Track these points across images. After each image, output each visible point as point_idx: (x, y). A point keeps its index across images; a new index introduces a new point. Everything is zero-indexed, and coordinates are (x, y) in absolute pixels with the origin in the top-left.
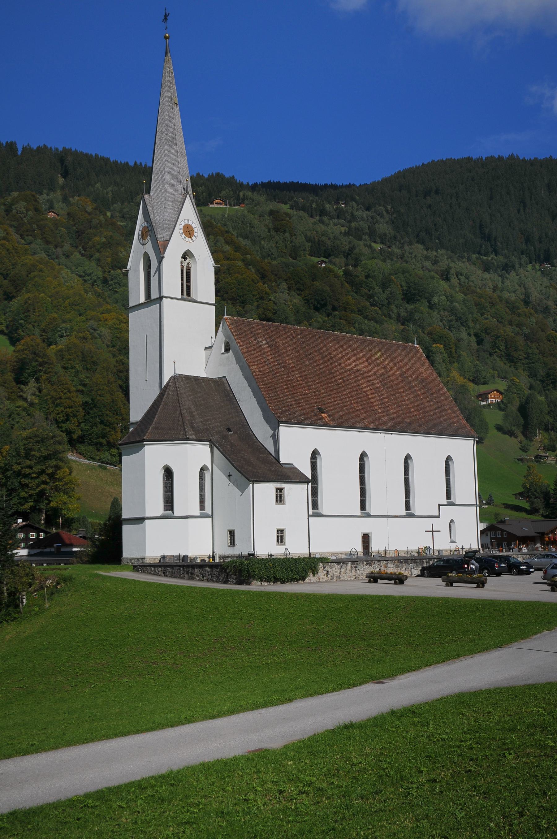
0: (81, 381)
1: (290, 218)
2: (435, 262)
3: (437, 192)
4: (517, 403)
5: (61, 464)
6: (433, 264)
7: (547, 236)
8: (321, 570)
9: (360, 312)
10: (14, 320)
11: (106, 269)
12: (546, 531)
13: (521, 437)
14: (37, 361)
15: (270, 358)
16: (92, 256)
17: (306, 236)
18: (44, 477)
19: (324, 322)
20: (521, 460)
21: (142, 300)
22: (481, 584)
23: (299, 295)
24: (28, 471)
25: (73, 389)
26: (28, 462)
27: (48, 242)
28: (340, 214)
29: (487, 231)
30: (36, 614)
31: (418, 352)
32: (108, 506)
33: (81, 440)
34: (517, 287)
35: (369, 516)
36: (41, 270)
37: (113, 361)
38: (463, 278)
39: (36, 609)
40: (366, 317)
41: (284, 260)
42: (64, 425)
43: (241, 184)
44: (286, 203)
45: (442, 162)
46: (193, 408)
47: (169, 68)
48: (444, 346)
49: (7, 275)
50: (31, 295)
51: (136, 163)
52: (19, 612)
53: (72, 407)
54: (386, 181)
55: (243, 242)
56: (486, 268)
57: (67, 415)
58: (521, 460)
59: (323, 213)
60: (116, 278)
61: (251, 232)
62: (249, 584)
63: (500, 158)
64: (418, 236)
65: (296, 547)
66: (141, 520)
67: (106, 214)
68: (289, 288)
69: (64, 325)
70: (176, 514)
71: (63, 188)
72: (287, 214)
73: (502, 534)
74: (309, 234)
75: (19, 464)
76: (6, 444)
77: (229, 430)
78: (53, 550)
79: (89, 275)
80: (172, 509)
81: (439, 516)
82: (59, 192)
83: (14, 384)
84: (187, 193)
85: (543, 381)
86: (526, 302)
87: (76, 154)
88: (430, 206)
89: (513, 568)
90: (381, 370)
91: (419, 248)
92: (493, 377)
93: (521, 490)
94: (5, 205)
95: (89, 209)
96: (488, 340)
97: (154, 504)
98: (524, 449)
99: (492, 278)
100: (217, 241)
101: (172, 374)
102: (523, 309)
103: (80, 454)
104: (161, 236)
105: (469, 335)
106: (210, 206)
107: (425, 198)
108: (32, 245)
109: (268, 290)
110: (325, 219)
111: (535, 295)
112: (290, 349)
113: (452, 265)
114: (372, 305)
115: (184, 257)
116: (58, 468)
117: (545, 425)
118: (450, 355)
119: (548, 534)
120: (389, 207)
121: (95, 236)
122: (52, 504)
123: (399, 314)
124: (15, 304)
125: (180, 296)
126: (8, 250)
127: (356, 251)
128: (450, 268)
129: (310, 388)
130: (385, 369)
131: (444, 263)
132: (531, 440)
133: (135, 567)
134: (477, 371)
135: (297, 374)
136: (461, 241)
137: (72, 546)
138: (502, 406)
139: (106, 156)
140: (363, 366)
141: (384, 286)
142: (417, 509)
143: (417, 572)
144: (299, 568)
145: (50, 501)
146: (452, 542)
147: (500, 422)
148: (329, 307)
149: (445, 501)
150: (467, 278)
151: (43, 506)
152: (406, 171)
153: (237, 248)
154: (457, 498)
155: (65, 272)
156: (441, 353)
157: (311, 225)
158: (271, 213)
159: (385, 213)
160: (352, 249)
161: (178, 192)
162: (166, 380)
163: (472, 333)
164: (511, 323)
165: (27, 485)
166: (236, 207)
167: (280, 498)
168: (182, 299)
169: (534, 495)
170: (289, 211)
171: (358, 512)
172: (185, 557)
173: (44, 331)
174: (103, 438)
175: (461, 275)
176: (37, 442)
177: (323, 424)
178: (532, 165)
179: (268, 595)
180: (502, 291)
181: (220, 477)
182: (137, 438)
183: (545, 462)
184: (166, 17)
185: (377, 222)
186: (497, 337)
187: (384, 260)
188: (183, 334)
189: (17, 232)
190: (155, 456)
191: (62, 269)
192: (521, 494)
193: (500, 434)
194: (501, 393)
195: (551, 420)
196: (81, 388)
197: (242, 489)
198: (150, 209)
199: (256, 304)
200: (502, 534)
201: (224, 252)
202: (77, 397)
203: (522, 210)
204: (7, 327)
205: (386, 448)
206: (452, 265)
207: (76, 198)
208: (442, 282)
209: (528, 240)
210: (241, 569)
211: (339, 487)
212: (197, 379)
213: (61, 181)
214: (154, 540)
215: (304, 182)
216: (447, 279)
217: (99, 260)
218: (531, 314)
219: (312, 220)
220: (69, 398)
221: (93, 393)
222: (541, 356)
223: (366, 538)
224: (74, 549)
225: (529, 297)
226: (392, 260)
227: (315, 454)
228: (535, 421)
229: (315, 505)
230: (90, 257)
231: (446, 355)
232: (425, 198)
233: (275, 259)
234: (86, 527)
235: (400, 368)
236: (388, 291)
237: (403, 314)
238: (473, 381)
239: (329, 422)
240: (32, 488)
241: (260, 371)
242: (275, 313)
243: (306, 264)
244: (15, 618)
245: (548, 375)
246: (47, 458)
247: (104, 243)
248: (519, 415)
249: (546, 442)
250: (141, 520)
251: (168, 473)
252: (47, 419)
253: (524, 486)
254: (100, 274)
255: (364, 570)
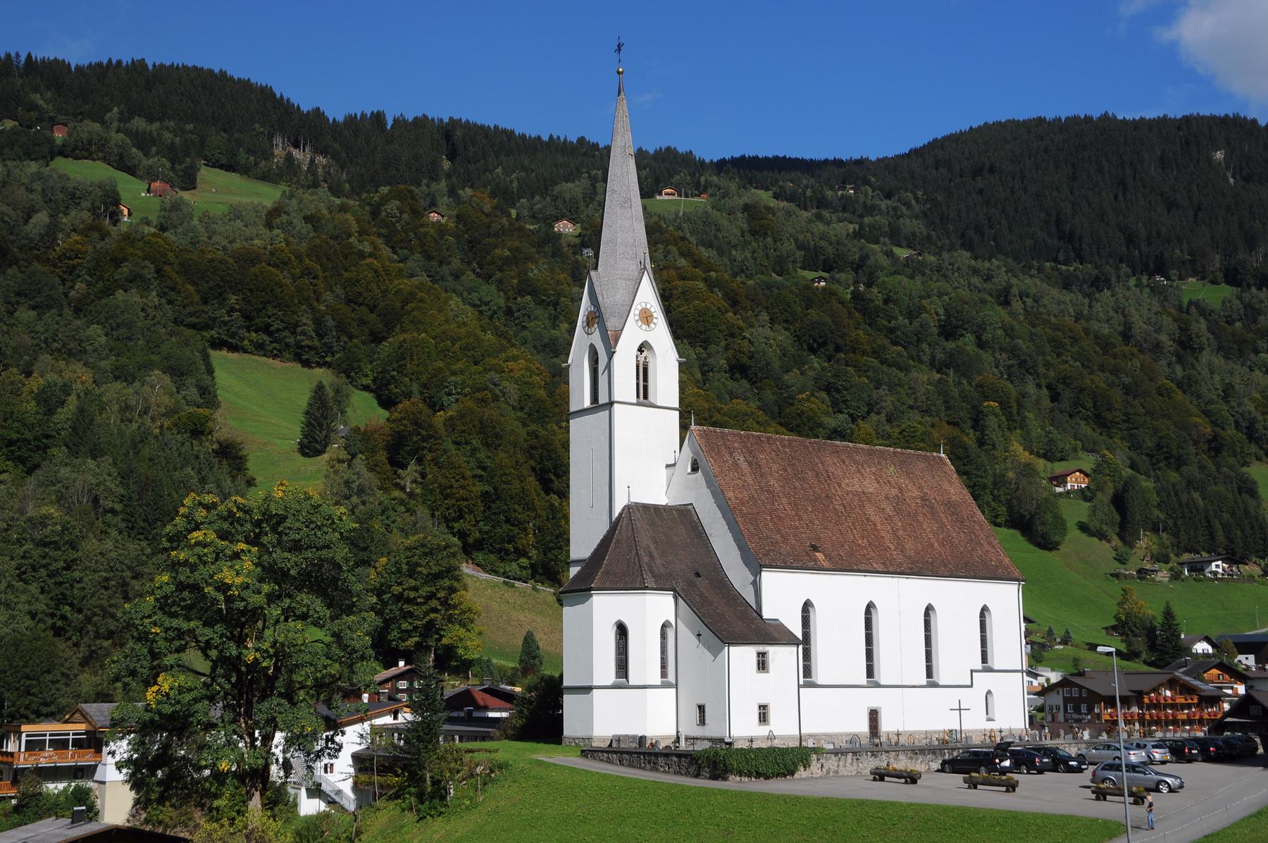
0: (480, 462)
1: (774, 214)
2: (988, 278)
3: (992, 170)
4: (1110, 490)
5: (456, 584)
6: (985, 281)
7: (1159, 234)
8: (814, 763)
9: (875, 354)
10: (384, 371)
11: (511, 293)
12: (1145, 689)
13: (1116, 541)
14: (419, 434)
15: (750, 480)
16: (491, 277)
17: (796, 241)
18: (434, 603)
19: (823, 369)
20: (1116, 576)
21: (587, 403)
22: (1011, 787)
23: (786, 329)
24: (412, 594)
25: (468, 473)
26: (412, 583)
27: (429, 258)
28: (846, 205)
29: (1067, 228)
30: (467, 808)
31: (945, 464)
32: (520, 642)
33: (479, 545)
34: (1112, 314)
35: (878, 685)
36: (422, 301)
37: (522, 432)
38: (1029, 301)
39: (468, 803)
40: (884, 362)
41: (764, 278)
42: (456, 525)
43: (702, 163)
44: (767, 189)
45: (999, 124)
46: (652, 547)
47: (623, 109)
48: (1001, 404)
49: (375, 307)
50: (407, 336)
51: (551, 137)
52: (446, 806)
53: (466, 500)
54: (915, 152)
55: (705, 253)
56: (1067, 286)
57: (460, 510)
58: (1116, 576)
59: (822, 203)
60: (524, 308)
61: (716, 237)
62: (726, 779)
63: (1088, 119)
64: (963, 235)
65: (783, 728)
66: (588, 689)
67: (510, 215)
68: (772, 321)
69: (453, 378)
70: (632, 682)
71: (449, 176)
72: (769, 209)
73: (1080, 693)
74: (801, 237)
75: (400, 584)
76: (383, 556)
77: (698, 575)
78: (462, 714)
79: (487, 304)
80: (626, 677)
81: (971, 686)
82: (443, 183)
83: (389, 467)
84: (645, 268)
85: (1151, 456)
86: (1126, 336)
87: (468, 126)
88: (981, 192)
89: (1059, 763)
90: (894, 492)
91: (963, 257)
92: (1075, 450)
93: (1114, 623)
94: (370, 205)
95: (487, 208)
96: (1067, 395)
97: (604, 670)
98: (1121, 560)
99: (1071, 299)
100: (668, 253)
101: (625, 502)
102: (1121, 348)
103: (478, 565)
104: (611, 324)
105: (1039, 386)
106: (658, 197)
107: (973, 179)
108: (409, 264)
109: (741, 323)
110: (826, 214)
111: (1139, 326)
112: (775, 467)
113: (1014, 281)
114: (895, 343)
115: (640, 350)
116: (452, 590)
117: (1154, 524)
118: (1010, 418)
119: (1148, 694)
120: (920, 193)
121: (496, 247)
122: (445, 641)
123: (934, 357)
124: (386, 348)
125: (634, 400)
126: (376, 272)
127: (871, 262)
128: (1011, 286)
129: (800, 519)
130: (900, 489)
131: (1002, 278)
132: (1132, 547)
133: (583, 751)
134: (1051, 441)
135: (784, 500)
136: (1029, 242)
137: (486, 708)
138: (1089, 494)
139: (509, 127)
140: (871, 486)
141: (912, 315)
142: (942, 676)
143: (936, 765)
144: (783, 760)
145: (442, 636)
146: (989, 720)
147: (1084, 519)
148: (831, 347)
149: (979, 666)
150: (1036, 301)
151: (432, 643)
152: (945, 139)
153: (697, 263)
154: (997, 661)
155: (455, 302)
156: (996, 415)
157: (804, 224)
158: (746, 208)
159: (913, 202)
160: (864, 258)
161: (633, 268)
162: (617, 511)
163: (1043, 382)
164: (1102, 368)
165: (411, 614)
166: (695, 199)
167: (762, 665)
168: (638, 404)
169: (1132, 631)
170: (773, 203)
171: (863, 679)
172: (642, 739)
173: (425, 386)
174: (509, 542)
175: (1028, 296)
176: (425, 554)
177: (818, 568)
178: (1136, 129)
179: (749, 796)
180: (1088, 320)
181: (687, 637)
182: (582, 589)
183: (1153, 580)
184: (619, 47)
185: (902, 215)
186: (1082, 390)
187: (912, 277)
188: (638, 446)
189: (387, 243)
190: (606, 608)
191: (451, 298)
192: (1114, 628)
193: (1084, 536)
194: (1086, 475)
195: (1162, 516)
196: (479, 472)
197: (715, 652)
198: (597, 289)
199: (723, 343)
200: (1080, 693)
201: (677, 268)
202: (474, 485)
203: (1120, 196)
204: (374, 380)
205: (901, 597)
206: (1014, 281)
207: (469, 191)
208: (999, 308)
209: (1130, 240)
210: (716, 760)
211: (837, 649)
212: (656, 508)
213: (446, 165)
214: (605, 715)
215: (793, 156)
216: (1006, 303)
217: (500, 282)
218: (1133, 355)
219: (805, 214)
220: (463, 487)
221: (496, 479)
222: (1148, 418)
223: (874, 716)
224: (491, 715)
225: (1130, 329)
226: (924, 274)
227: (807, 606)
228: (1138, 517)
229: (807, 672)
230: (487, 278)
231: (1003, 418)
232: (973, 179)
233: (750, 277)
234: (491, 673)
235: (920, 488)
236: (916, 324)
237: (940, 356)
238: (1045, 456)
239: (826, 564)
240: (418, 618)
241: (737, 498)
242: (751, 357)
243: (796, 284)
244: (441, 813)
245: (1159, 447)
246: (438, 576)
247: (507, 257)
248: (1113, 508)
249: (1155, 548)
250: (588, 689)
251: (622, 630)
252: (433, 516)
253: (1117, 618)
254: (502, 302)
255: (869, 764)
